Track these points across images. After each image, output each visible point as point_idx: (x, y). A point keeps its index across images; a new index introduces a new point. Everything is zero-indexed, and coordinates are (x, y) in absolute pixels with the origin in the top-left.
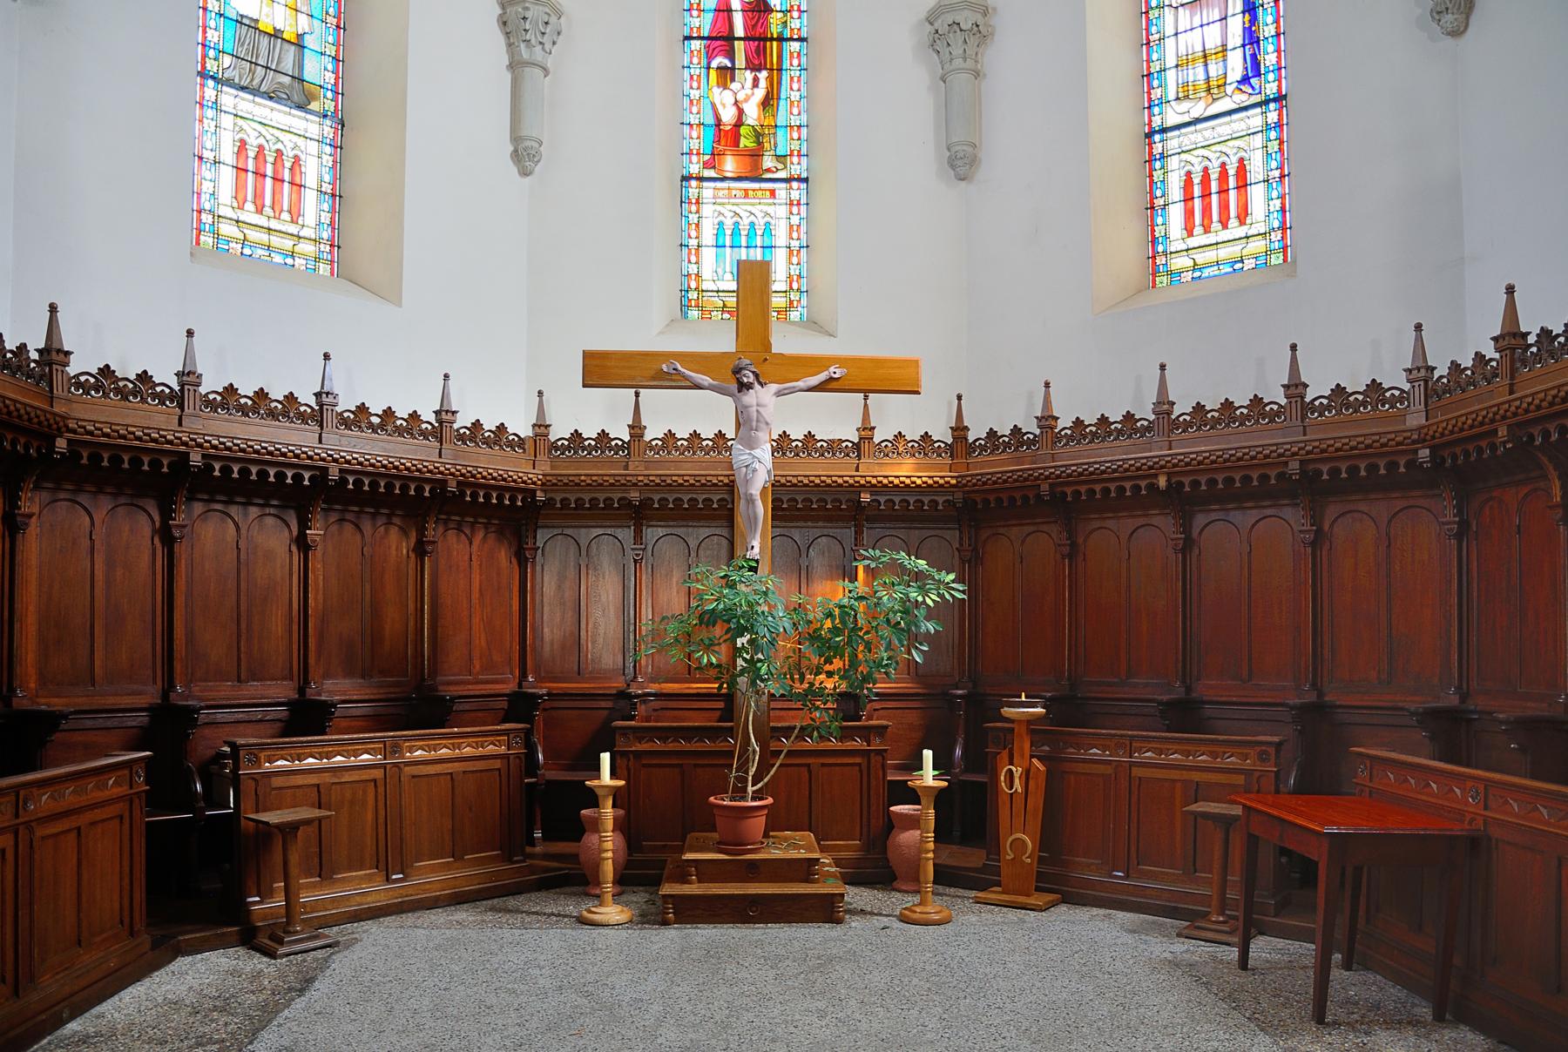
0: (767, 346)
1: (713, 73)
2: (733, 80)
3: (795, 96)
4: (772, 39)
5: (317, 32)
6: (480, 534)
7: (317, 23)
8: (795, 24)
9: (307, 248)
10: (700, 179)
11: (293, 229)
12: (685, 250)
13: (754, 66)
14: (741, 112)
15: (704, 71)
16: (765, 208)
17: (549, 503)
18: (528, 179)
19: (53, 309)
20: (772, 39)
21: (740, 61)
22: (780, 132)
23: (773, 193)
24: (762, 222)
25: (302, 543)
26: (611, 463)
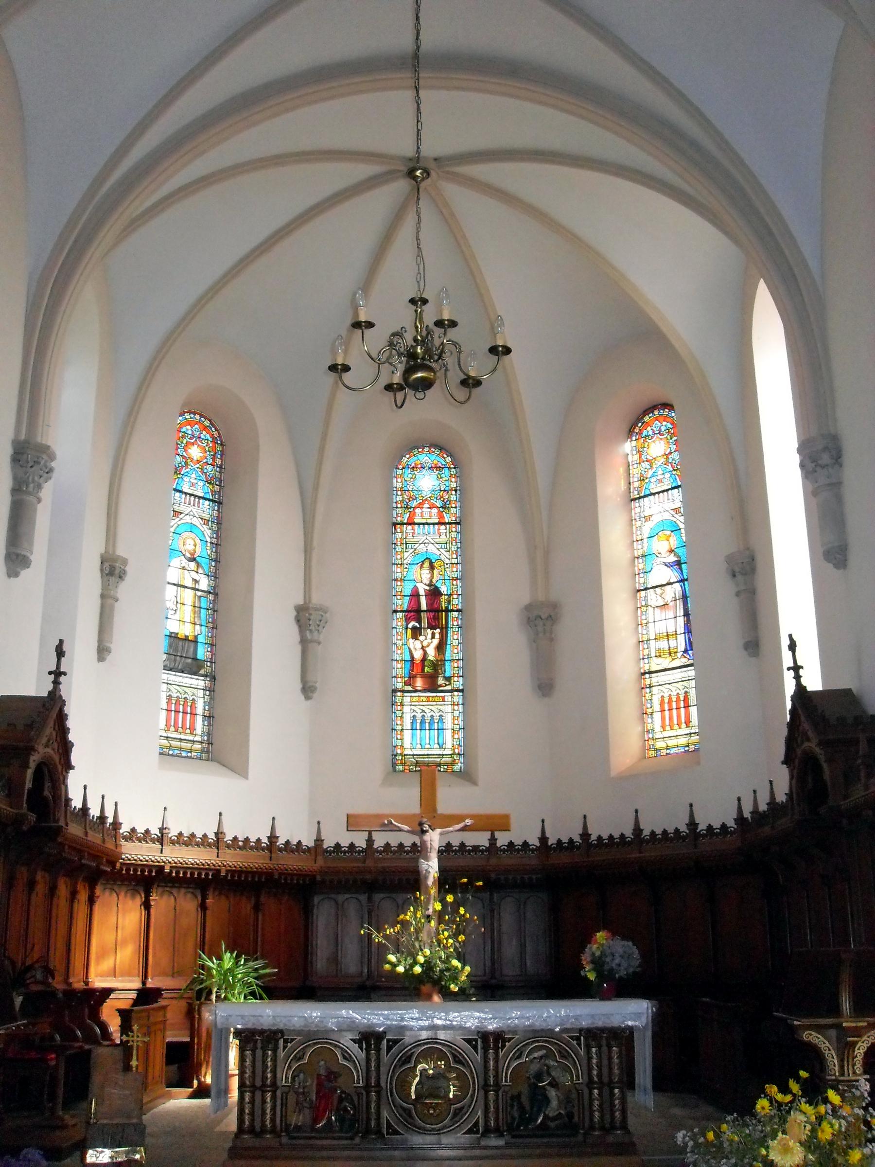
0: (435, 810)
1: (409, 631)
2: (420, 635)
3: (455, 642)
4: (443, 611)
5: (204, 633)
6: (286, 898)
7: (203, 628)
8: (455, 602)
9: (198, 746)
10: (403, 691)
11: (191, 738)
12: (394, 732)
13: (432, 627)
14: (425, 653)
15: (404, 630)
16: (439, 707)
17: (323, 882)
18: (309, 702)
19: (116, 804)
20: (443, 611)
21: (425, 624)
22: (447, 663)
23: (444, 700)
24: (438, 715)
25: (203, 907)
26: (357, 860)
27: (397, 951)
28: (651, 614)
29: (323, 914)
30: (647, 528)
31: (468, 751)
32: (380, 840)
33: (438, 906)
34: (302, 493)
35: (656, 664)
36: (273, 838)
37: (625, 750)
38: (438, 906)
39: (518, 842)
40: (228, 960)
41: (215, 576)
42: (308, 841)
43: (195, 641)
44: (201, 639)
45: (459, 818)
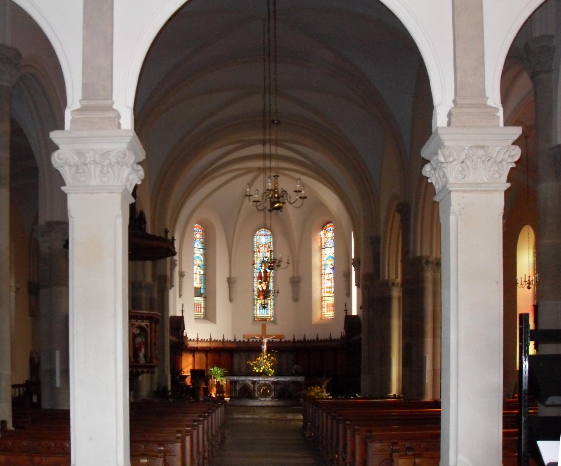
27: (256, 366)
28: (325, 281)
29: (236, 358)
30: (326, 257)
31: (275, 316)
32: (251, 340)
33: (266, 357)
34: (228, 244)
35: (326, 295)
36: (224, 339)
37: (316, 318)
38: (266, 357)
39: (287, 340)
40: (216, 368)
41: (205, 270)
42: (232, 340)
43: (201, 288)
44: (202, 288)
45: (271, 336)
